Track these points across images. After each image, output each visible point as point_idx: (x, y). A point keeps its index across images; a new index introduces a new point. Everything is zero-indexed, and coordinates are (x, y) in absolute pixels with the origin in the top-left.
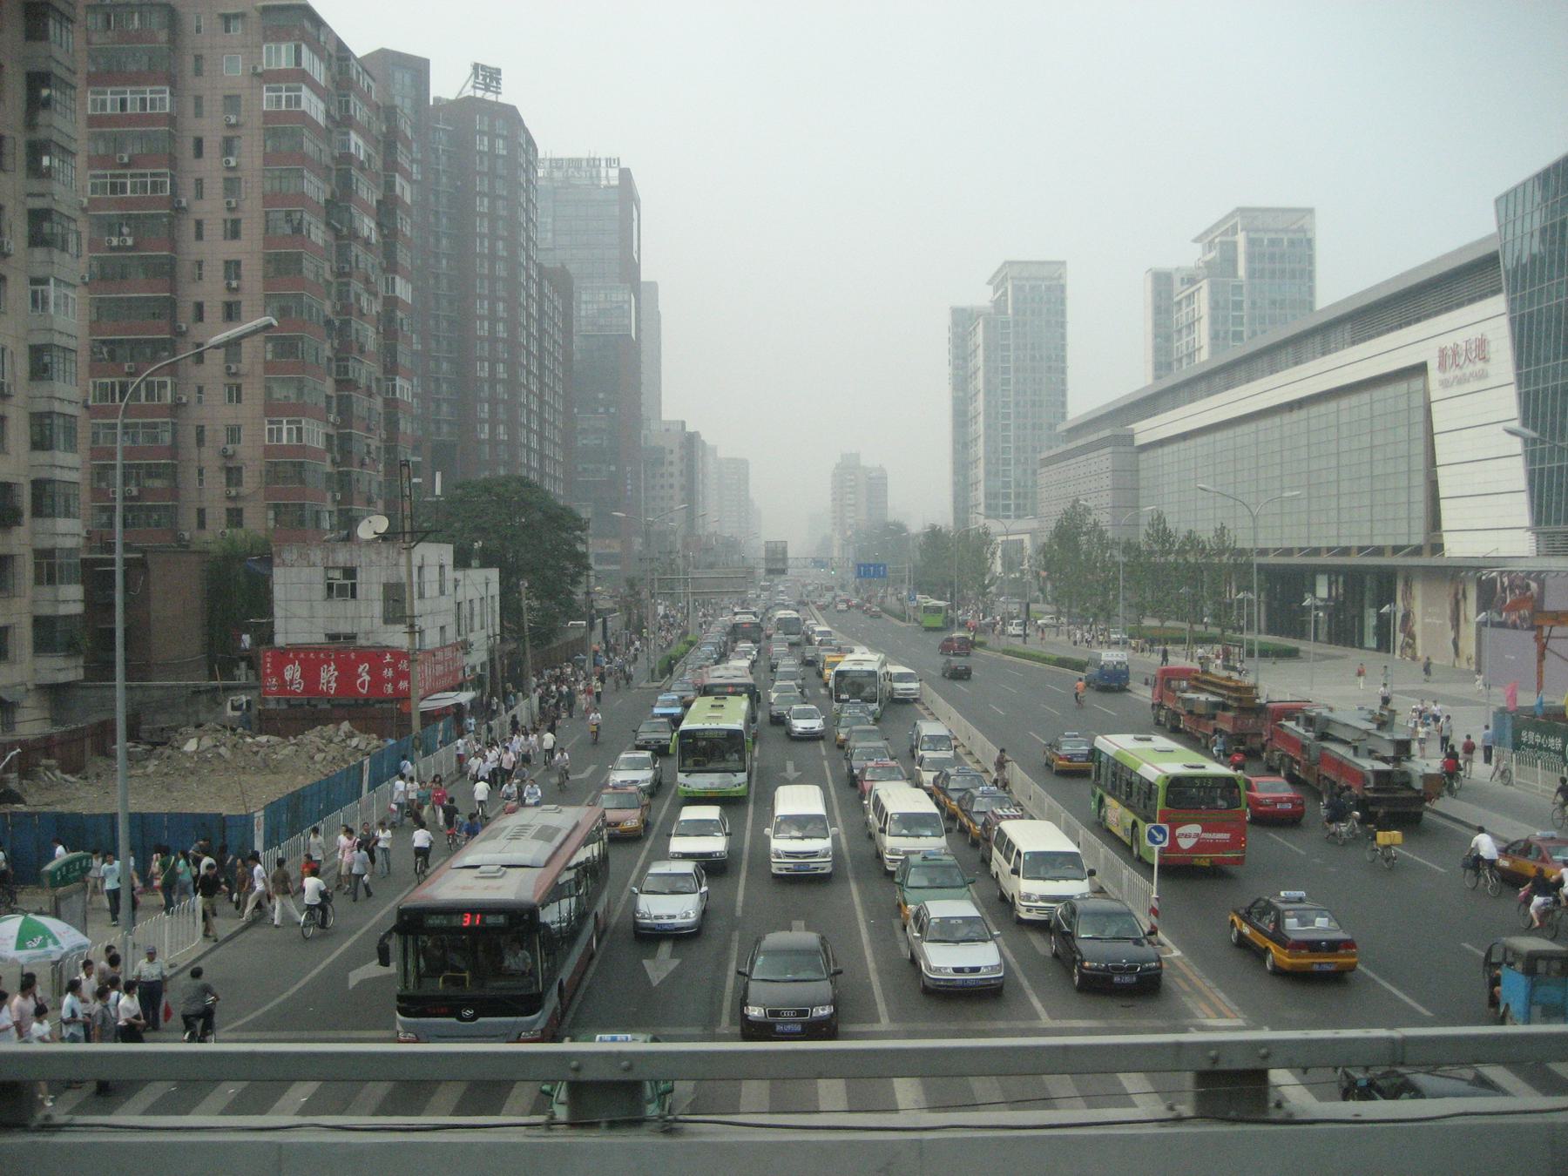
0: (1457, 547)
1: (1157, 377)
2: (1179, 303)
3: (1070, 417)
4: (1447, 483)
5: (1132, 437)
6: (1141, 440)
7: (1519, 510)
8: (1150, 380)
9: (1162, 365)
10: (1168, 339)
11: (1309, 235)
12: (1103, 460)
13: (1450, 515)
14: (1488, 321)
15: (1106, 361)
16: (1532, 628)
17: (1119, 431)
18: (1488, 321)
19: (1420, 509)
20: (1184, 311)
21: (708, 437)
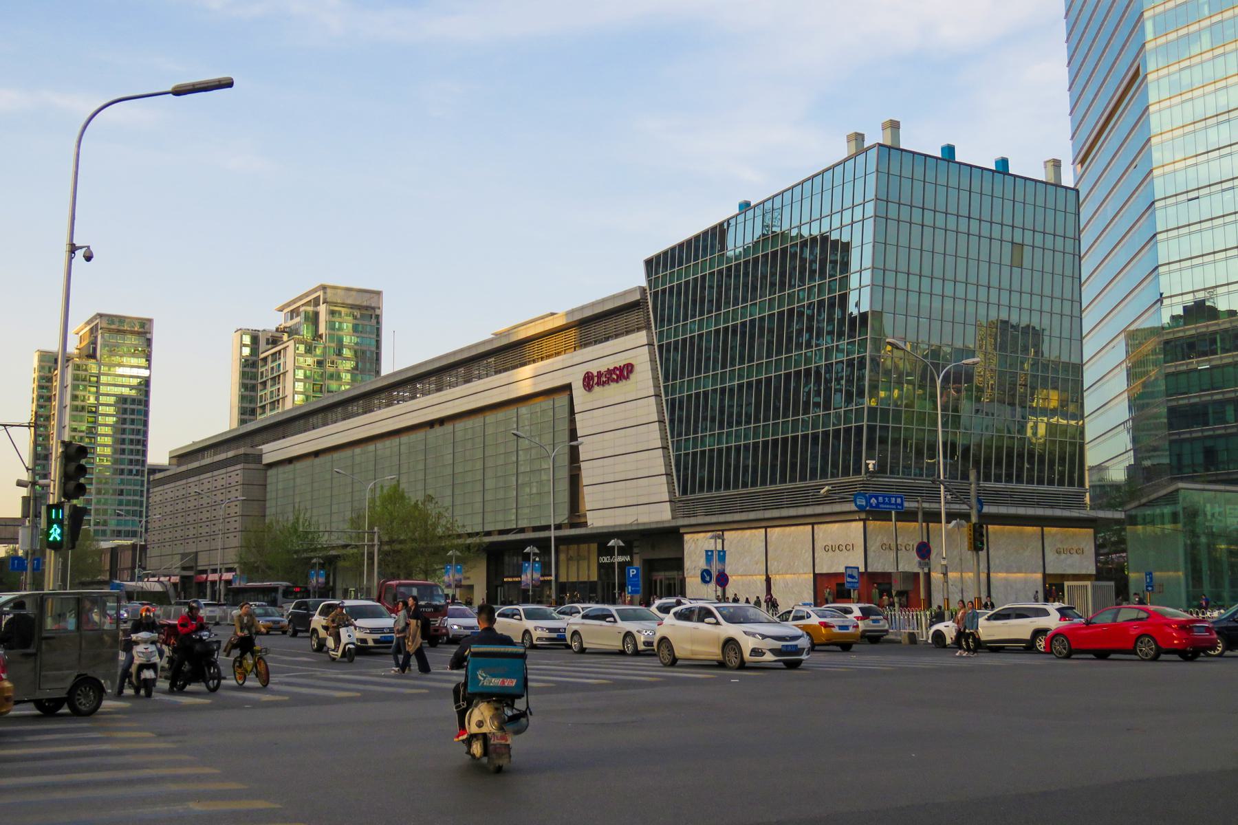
0: (596, 521)
1: (243, 422)
2: (265, 359)
3: (384, 372)
4: (587, 476)
5: (260, 456)
6: (267, 459)
7: (660, 489)
8: (235, 425)
9: (248, 410)
10: (253, 388)
11: (378, 312)
12: (236, 474)
13: (590, 498)
14: (634, 348)
15: (191, 407)
16: (1045, 367)
17: (249, 451)
18: (634, 348)
19: (564, 497)
20: (270, 365)
21: (739, 160)
